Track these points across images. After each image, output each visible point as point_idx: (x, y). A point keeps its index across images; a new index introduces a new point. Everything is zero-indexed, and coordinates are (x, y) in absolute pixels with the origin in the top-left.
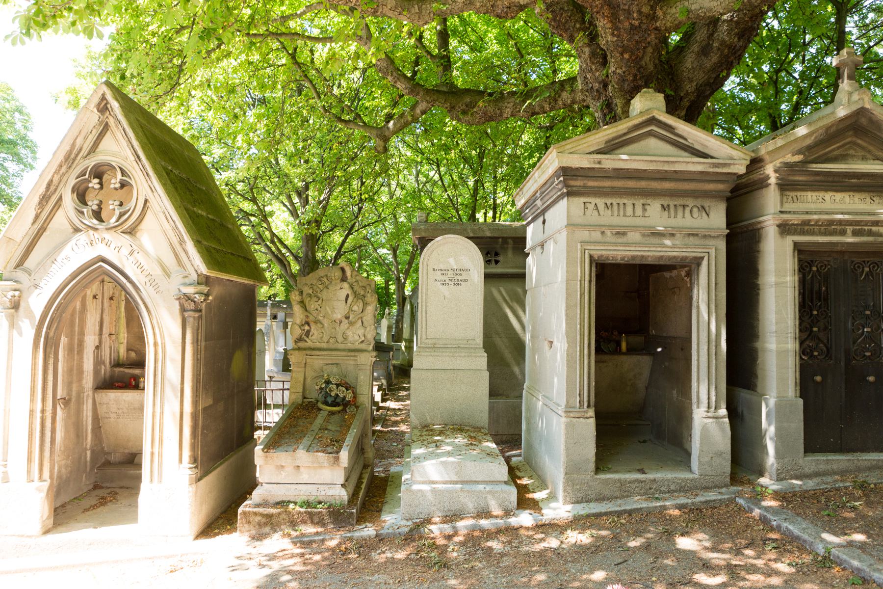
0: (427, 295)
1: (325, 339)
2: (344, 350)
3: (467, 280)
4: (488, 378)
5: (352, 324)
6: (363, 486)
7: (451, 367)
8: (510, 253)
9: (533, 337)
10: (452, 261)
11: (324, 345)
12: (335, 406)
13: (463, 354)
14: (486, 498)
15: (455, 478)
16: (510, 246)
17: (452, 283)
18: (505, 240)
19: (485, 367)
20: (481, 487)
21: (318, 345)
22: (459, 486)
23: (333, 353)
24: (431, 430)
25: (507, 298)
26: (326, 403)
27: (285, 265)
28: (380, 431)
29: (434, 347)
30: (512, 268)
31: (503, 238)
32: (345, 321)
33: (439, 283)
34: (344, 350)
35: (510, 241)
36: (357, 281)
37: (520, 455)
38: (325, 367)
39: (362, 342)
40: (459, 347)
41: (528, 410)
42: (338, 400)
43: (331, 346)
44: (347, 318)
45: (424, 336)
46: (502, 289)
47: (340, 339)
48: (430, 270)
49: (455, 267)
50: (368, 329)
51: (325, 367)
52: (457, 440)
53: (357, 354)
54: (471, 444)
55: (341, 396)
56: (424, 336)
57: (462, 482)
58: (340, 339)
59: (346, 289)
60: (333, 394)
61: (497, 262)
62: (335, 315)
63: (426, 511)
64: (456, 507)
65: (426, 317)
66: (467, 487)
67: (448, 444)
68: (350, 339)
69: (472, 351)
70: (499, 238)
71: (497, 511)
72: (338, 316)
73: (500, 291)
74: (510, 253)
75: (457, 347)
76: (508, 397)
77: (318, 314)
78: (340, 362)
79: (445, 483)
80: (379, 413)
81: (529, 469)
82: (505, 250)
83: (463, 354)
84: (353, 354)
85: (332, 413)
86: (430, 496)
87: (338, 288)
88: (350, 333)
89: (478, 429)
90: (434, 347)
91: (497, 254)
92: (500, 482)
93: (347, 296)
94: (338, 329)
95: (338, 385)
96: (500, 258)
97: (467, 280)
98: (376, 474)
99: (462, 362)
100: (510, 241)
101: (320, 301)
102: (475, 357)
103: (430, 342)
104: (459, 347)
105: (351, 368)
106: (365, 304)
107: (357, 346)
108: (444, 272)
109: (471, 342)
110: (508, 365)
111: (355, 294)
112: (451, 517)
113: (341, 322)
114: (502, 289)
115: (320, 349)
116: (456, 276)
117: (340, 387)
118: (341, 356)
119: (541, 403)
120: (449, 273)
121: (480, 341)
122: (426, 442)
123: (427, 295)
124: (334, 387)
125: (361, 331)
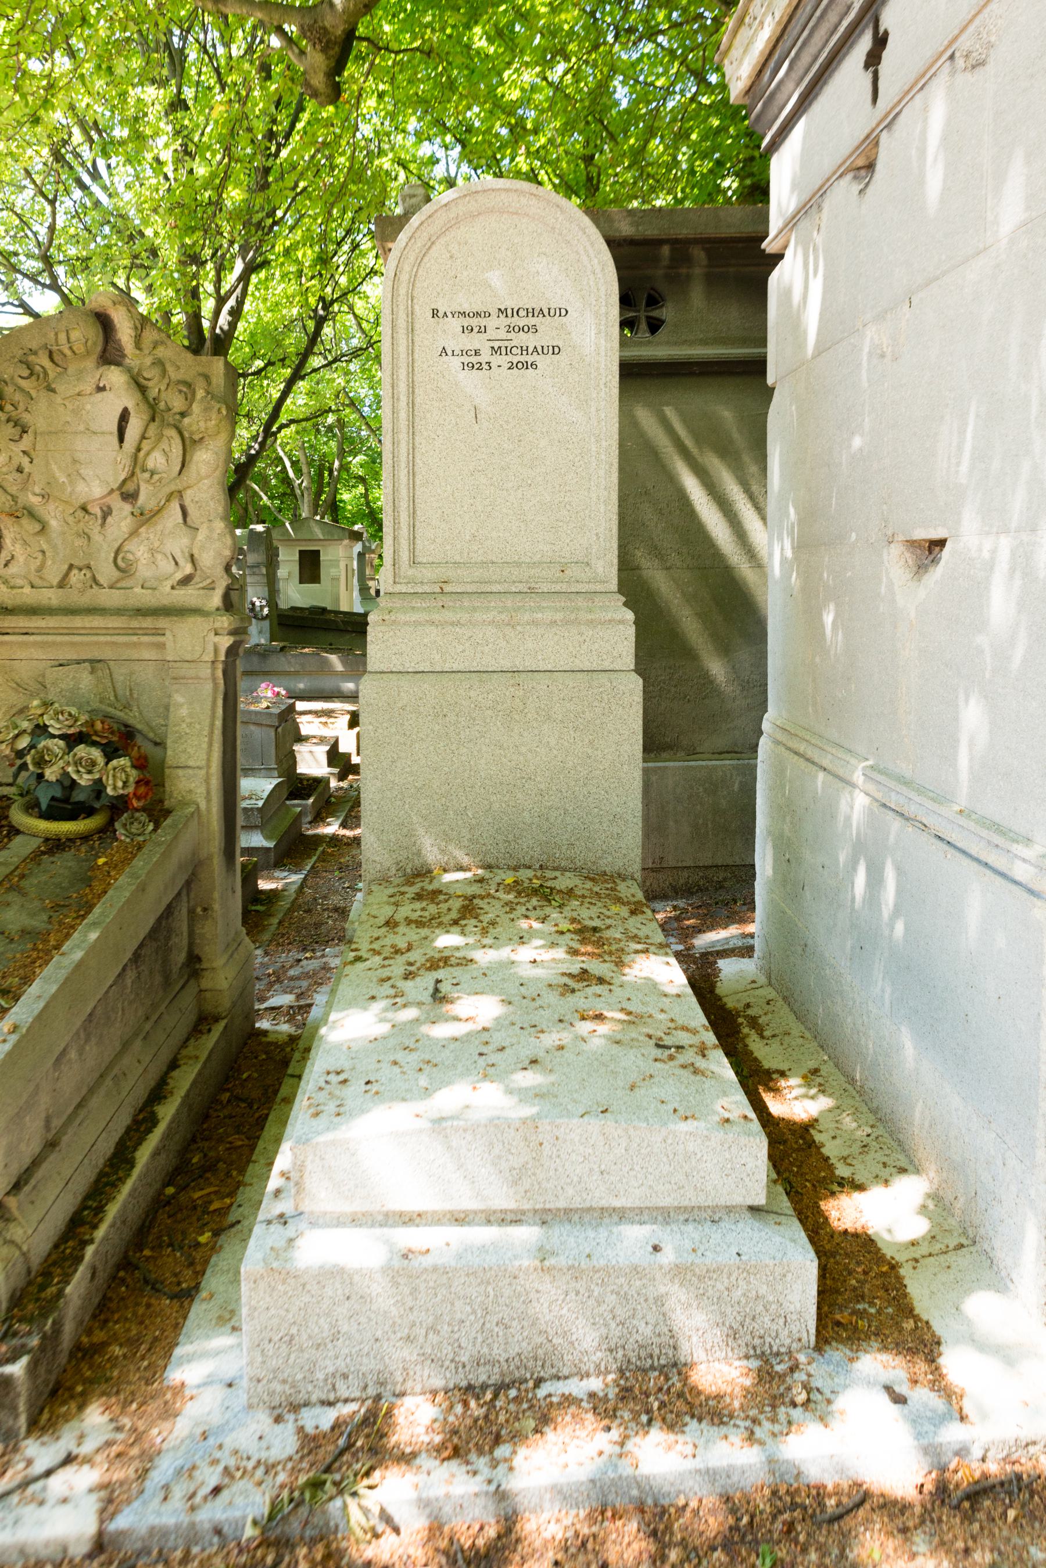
0: (412, 405)
1: (54, 573)
2: (119, 612)
3: (556, 350)
4: (638, 698)
5: (145, 518)
6: (167, 1112)
7: (507, 665)
8: (697, 296)
9: (807, 546)
10: (495, 278)
11: (51, 597)
12: (72, 817)
13: (548, 616)
14: (660, 1301)
15: (503, 1199)
16: (697, 271)
17: (503, 360)
18: (681, 247)
19: (629, 661)
20: (635, 1237)
21: (27, 595)
22: (527, 1234)
23: (78, 622)
24: (434, 895)
25: (689, 443)
26: (32, 807)
27: (721, 753)
28: (334, 840)
29: (442, 593)
30: (704, 342)
31: (674, 242)
32: (122, 510)
33: (456, 362)
34: (119, 612)
35: (699, 254)
36: (159, 363)
37: (747, 951)
38: (52, 674)
39: (186, 581)
40: (532, 591)
41: (785, 809)
42: (79, 796)
43: (75, 597)
44: (130, 497)
45: (404, 556)
46: (669, 412)
47: (106, 572)
48: (423, 314)
49: (510, 304)
50: (201, 536)
51: (52, 674)
52: (525, 954)
53: (162, 623)
54: (584, 975)
55: (84, 780)
56: (404, 556)
57: (545, 1218)
58: (106, 572)
59: (118, 393)
60: (51, 774)
61: (655, 326)
62: (81, 487)
63: (369, 1365)
64: (509, 1347)
65: (413, 487)
66: (571, 1242)
67: (488, 981)
68: (144, 571)
69: (580, 602)
70: (658, 242)
71: (720, 1372)
72: (94, 488)
73: (666, 419)
74: (697, 296)
75: (519, 592)
76: (692, 752)
77: (24, 489)
78: (107, 654)
79: (460, 1219)
80: (344, 784)
81: (796, 1029)
82: (679, 282)
83: (548, 616)
84: (148, 623)
85: (55, 845)
86: (383, 1297)
87: (88, 387)
88: (139, 551)
89: (603, 881)
90: (442, 593)
91: (654, 301)
92: (729, 1209)
93: (124, 417)
94: (96, 537)
95: (73, 740)
96: (667, 313)
97: (556, 350)
98: (263, 1024)
99: (548, 645)
100: (699, 254)
101: (26, 442)
102: (590, 623)
103: (428, 574)
104: (532, 591)
105: (146, 675)
106: (189, 444)
107: (167, 595)
108: (473, 320)
109: (572, 572)
110: (689, 654)
111: (154, 411)
112: (494, 1413)
113: (107, 513)
114: (669, 412)
115: (33, 611)
116: (517, 337)
117: (82, 751)
118: (107, 631)
119: (861, 801)
120: (492, 323)
121: (606, 567)
122: (398, 967)
123: (412, 405)
124: (57, 746)
125: (178, 544)
